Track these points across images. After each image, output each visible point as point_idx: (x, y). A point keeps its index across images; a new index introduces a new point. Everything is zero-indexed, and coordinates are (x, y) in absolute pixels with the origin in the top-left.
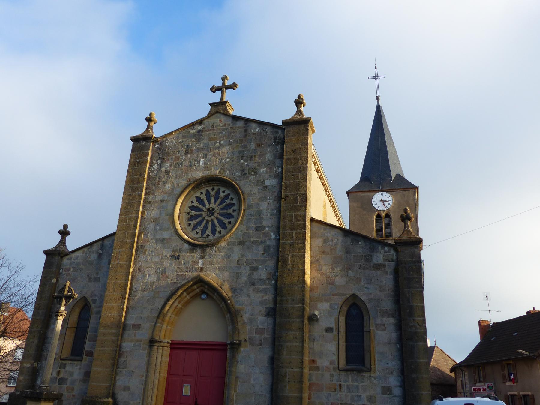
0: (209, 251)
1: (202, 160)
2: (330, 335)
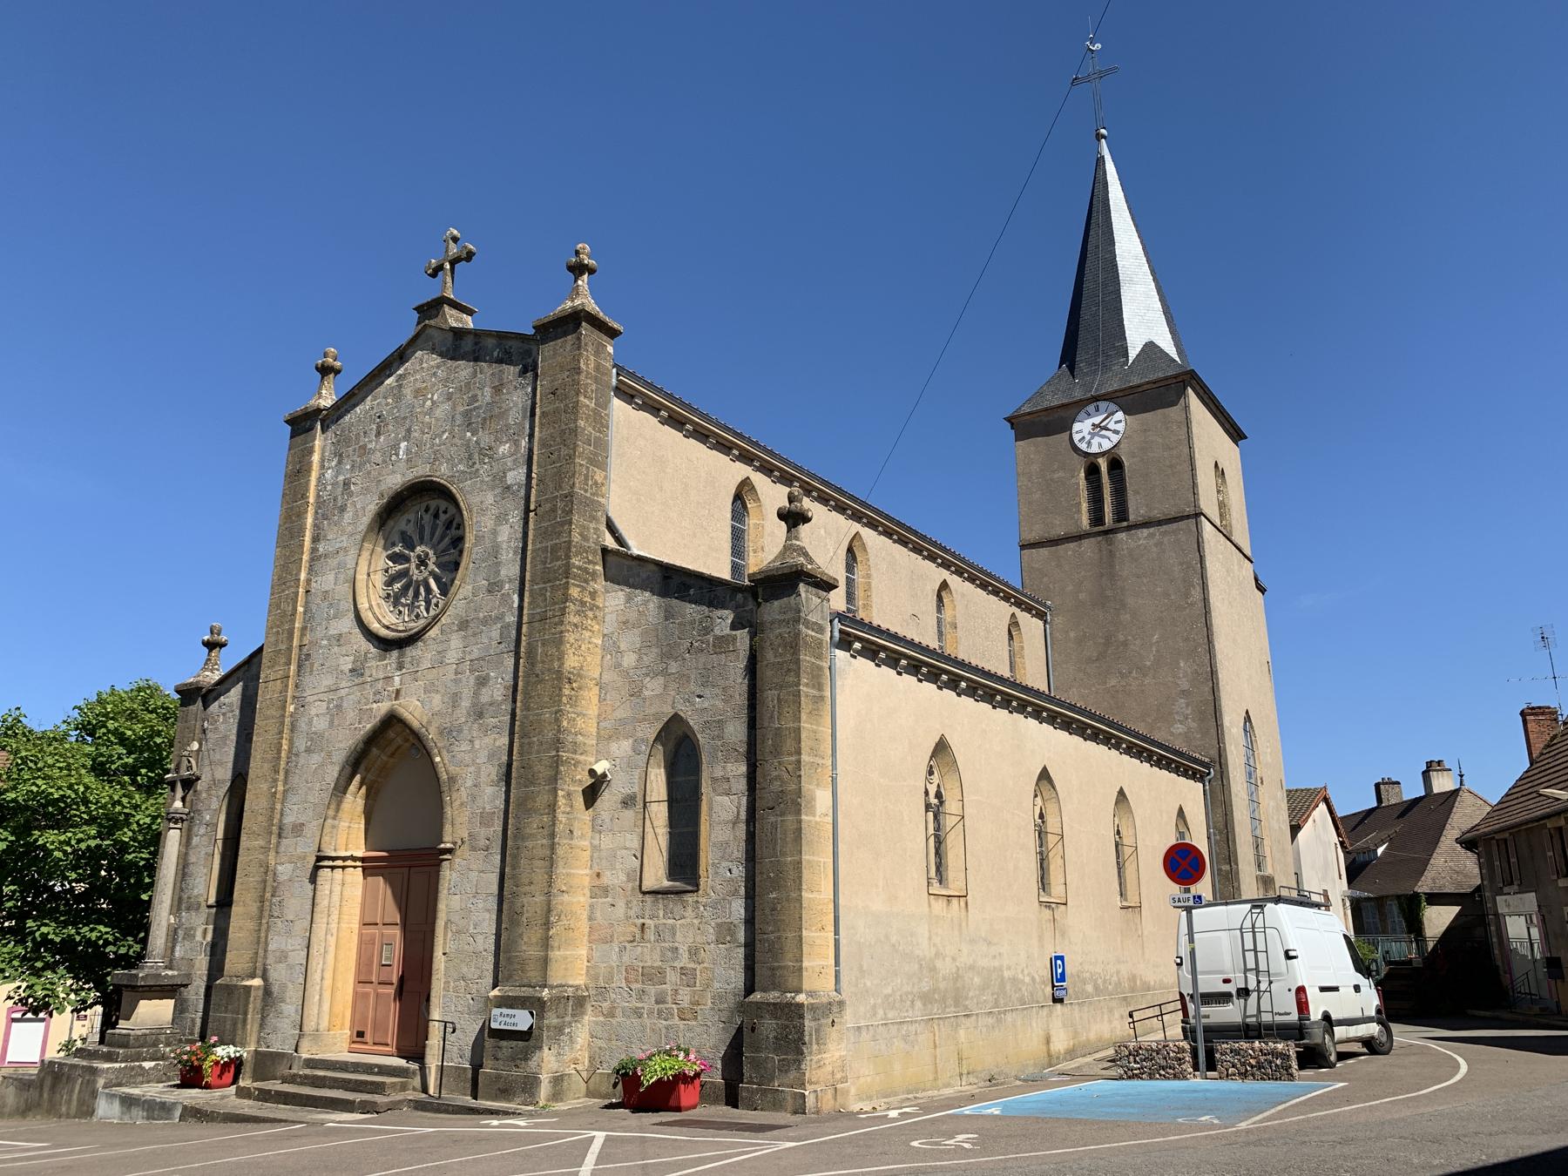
0: (410, 652)
1: (403, 445)
2: (629, 814)
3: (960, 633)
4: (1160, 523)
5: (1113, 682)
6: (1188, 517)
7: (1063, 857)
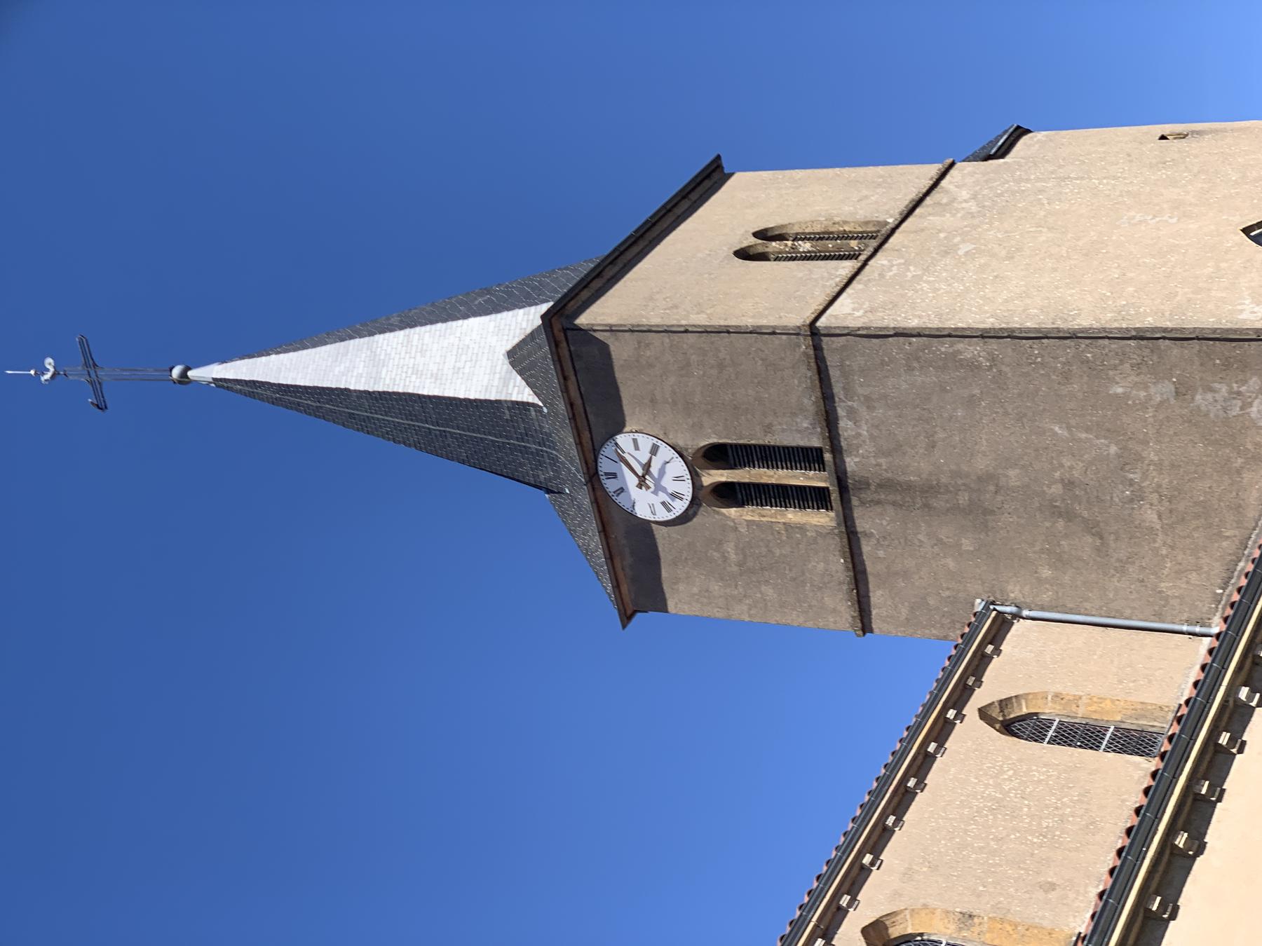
3: (981, 907)
4: (827, 398)
5: (1151, 516)
6: (817, 348)
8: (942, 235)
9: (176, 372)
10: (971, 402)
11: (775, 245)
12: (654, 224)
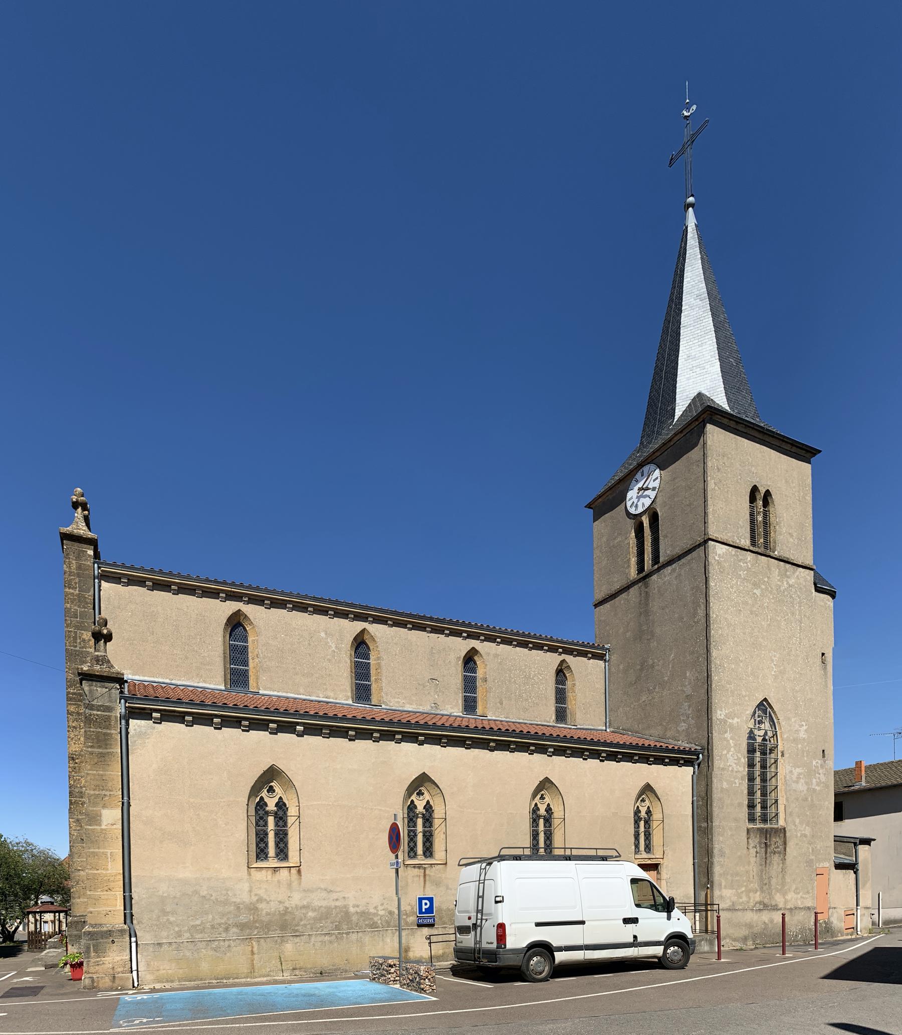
3: (490, 683)
4: (680, 557)
5: (644, 698)
6: (699, 545)
7: (446, 833)
8: (766, 579)
9: (691, 199)
10: (681, 618)
11: (760, 503)
12: (773, 437)
